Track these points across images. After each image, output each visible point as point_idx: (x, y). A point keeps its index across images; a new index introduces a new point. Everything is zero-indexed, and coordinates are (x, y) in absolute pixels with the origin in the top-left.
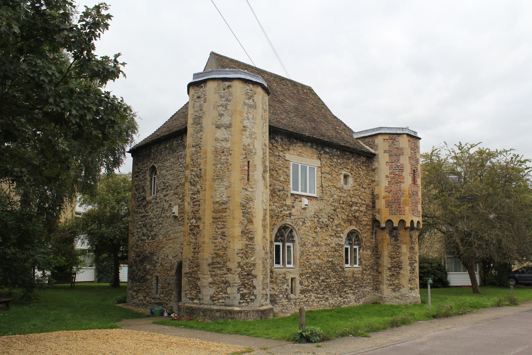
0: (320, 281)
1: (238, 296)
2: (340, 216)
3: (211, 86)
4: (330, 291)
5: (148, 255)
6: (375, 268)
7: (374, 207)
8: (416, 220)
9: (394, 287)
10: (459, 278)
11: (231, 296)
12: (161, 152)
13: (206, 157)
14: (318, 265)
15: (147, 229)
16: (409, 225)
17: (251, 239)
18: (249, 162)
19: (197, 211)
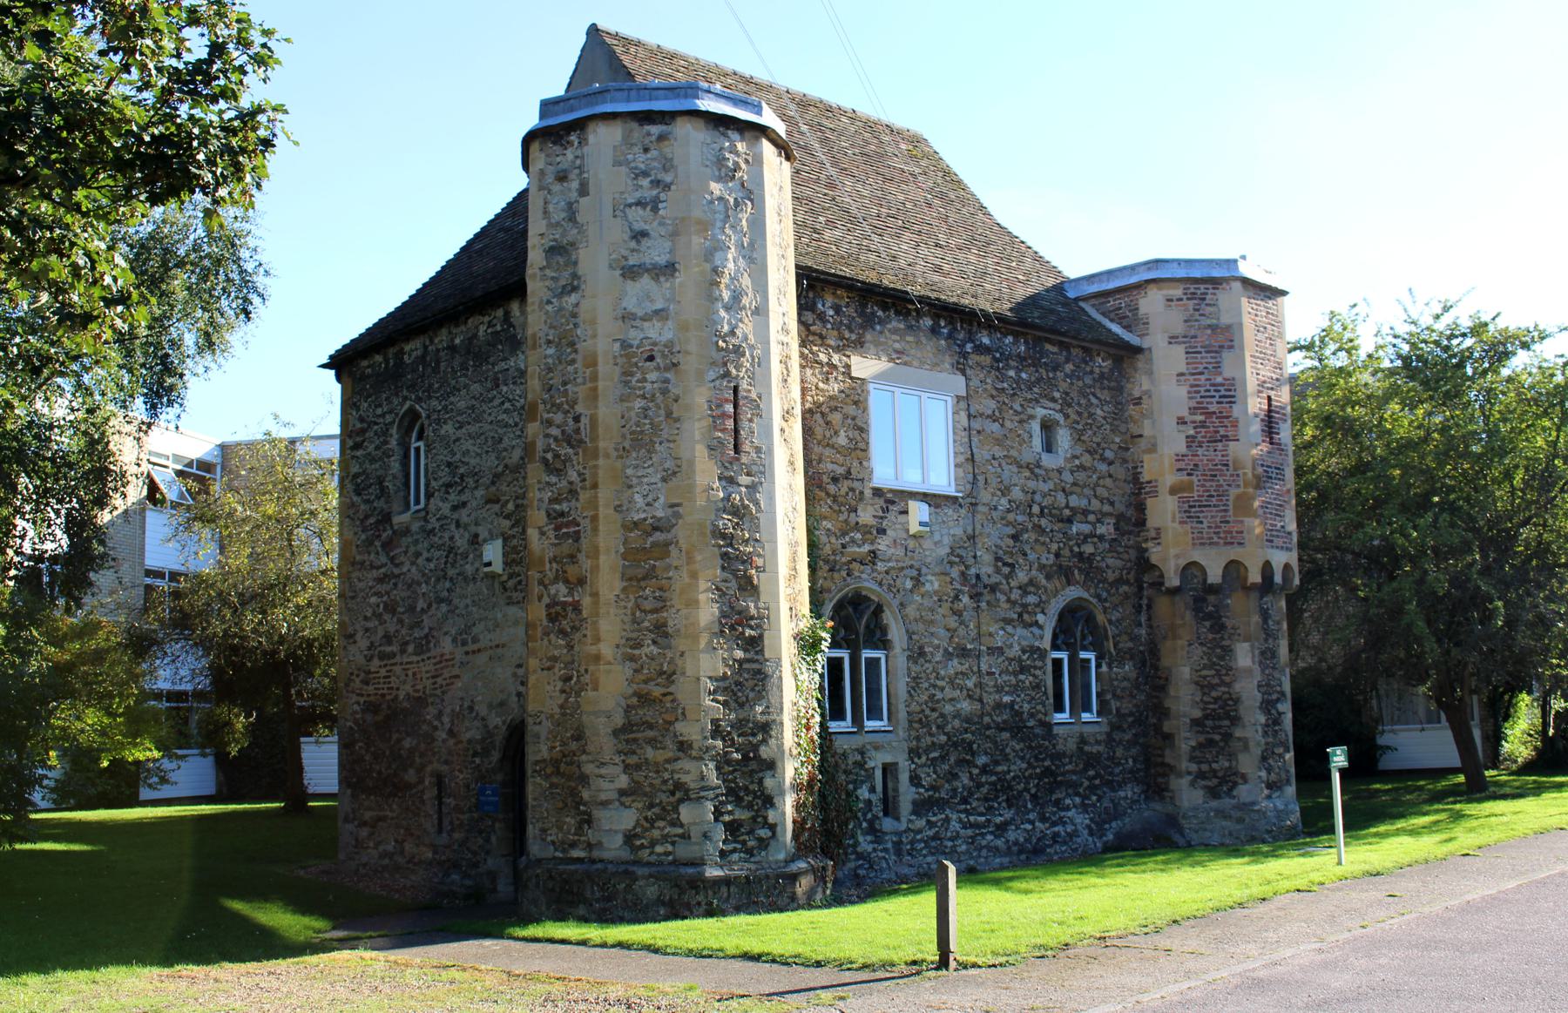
0: (975, 771)
1: (720, 833)
2: (1032, 556)
3: (604, 138)
4: (1007, 800)
5: (406, 704)
7: (1141, 523)
9: (1215, 781)
11: (695, 833)
12: (438, 362)
13: (594, 378)
14: (968, 720)
15: (401, 621)
18: (736, 389)
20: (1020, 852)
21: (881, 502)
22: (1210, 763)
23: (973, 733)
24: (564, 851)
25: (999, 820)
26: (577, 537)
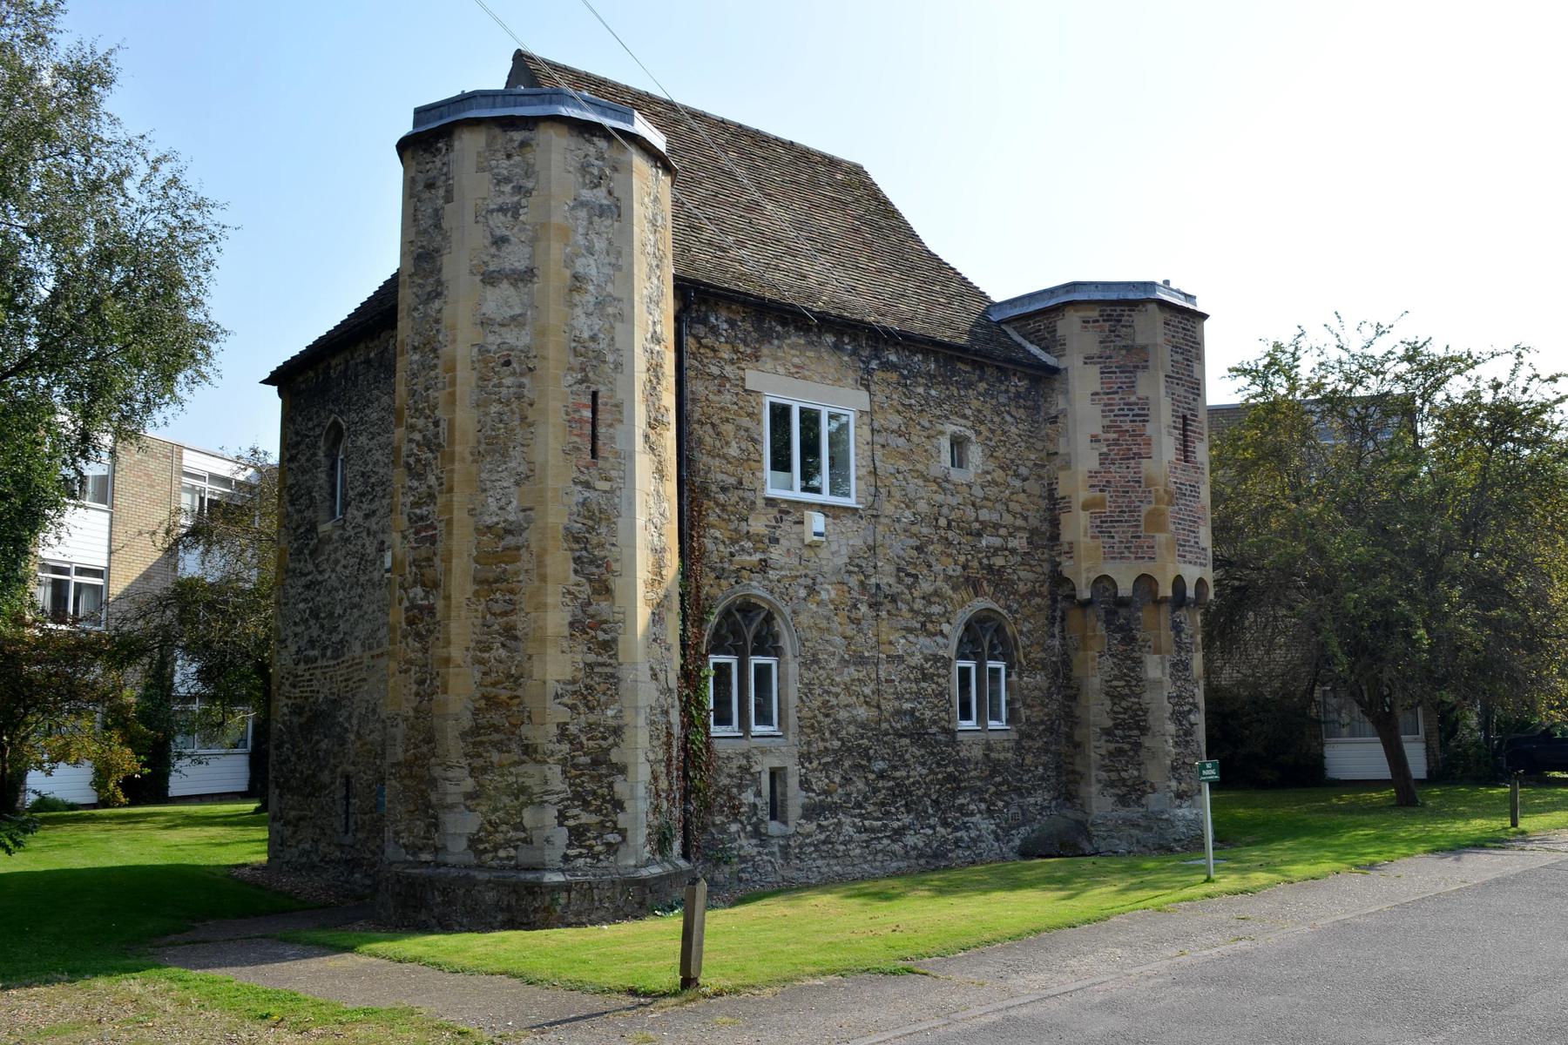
2: (938, 568)
4: (906, 805)
5: (324, 707)
6: (1064, 729)
7: (1055, 538)
8: (1191, 574)
9: (1124, 789)
10: (1355, 756)
12: (357, 377)
13: (453, 383)
14: (863, 726)
15: (322, 627)
16: (1169, 593)
17: (608, 646)
18: (595, 395)
19: (429, 559)
20: (919, 856)
21: (775, 512)
22: (1118, 771)
23: (869, 739)
24: (414, 854)
25: (896, 824)
26: (433, 540)
